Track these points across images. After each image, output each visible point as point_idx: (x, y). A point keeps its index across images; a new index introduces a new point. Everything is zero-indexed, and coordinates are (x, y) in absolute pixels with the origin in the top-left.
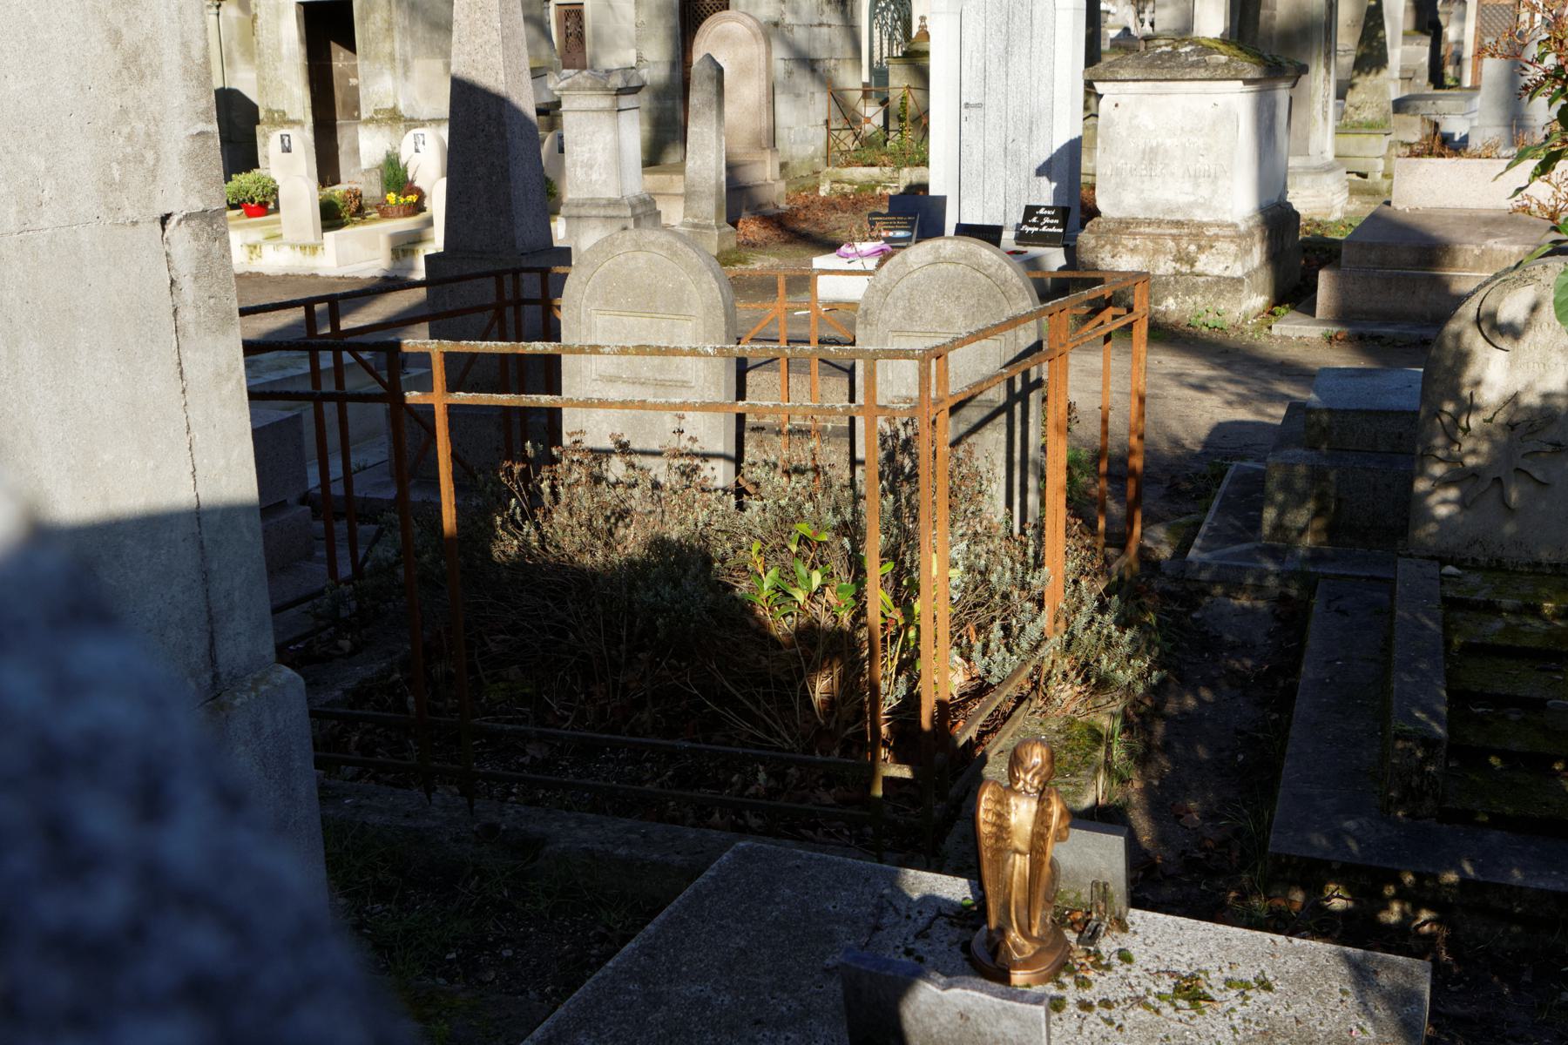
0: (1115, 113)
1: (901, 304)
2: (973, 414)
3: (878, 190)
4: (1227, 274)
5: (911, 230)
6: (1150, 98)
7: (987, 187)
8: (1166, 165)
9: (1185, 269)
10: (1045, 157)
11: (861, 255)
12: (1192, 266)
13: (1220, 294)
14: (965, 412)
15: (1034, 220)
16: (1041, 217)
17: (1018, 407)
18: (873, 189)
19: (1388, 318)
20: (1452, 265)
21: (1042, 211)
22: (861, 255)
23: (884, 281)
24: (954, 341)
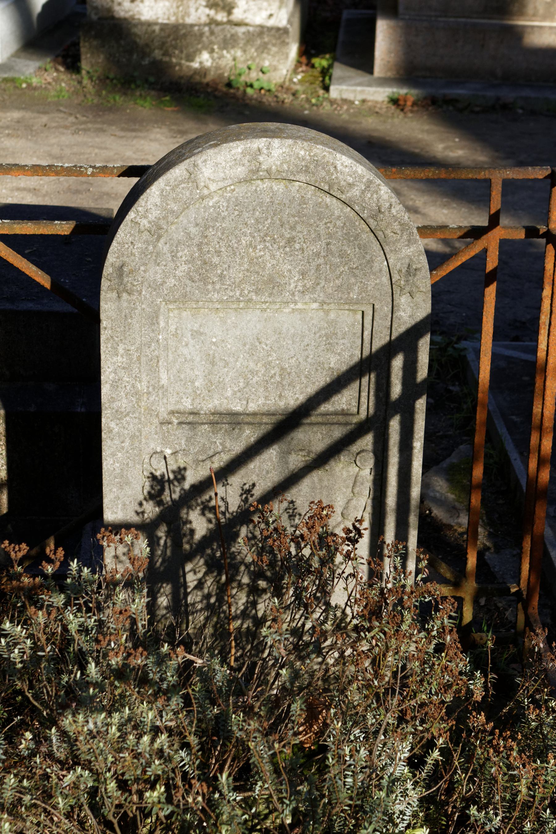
1: (184, 253)
2: (314, 437)
4: (271, 23)
9: (221, 17)
12: (230, 13)
13: (264, 48)
14: (300, 435)
17: (395, 424)
19: (455, 76)
20: (521, 13)
23: (154, 214)
24: (50, 166)
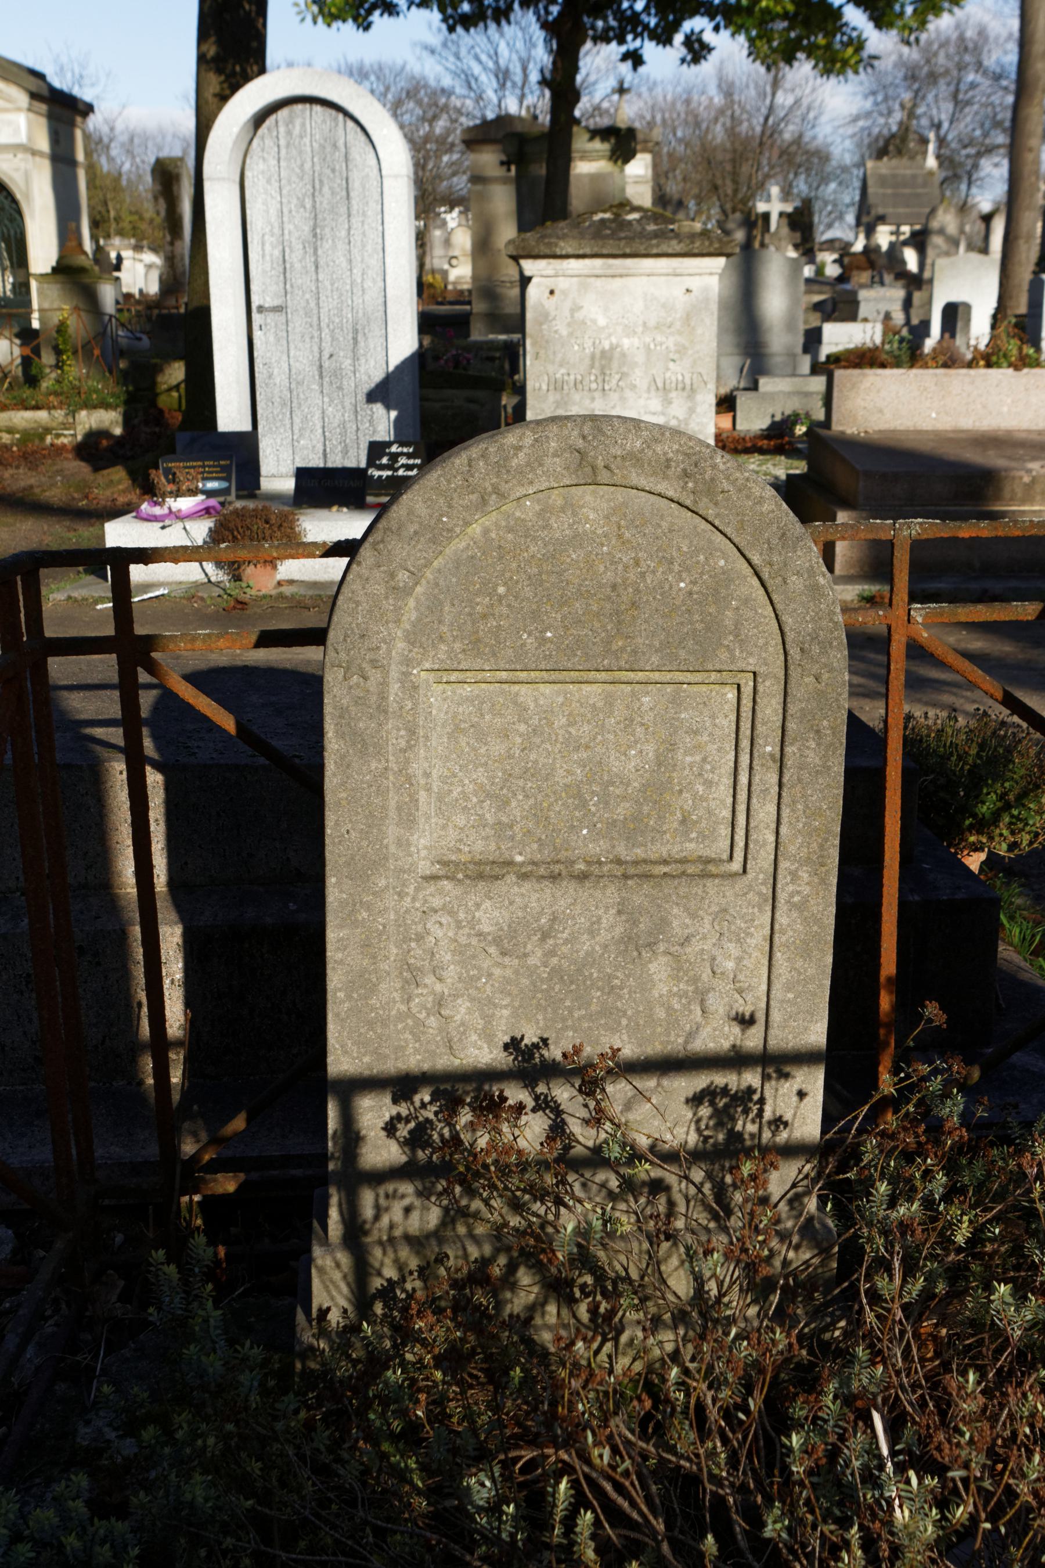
0: (550, 304)
3: (49, 439)
5: (227, 479)
6: (599, 283)
7: (297, 420)
8: (623, 376)
10: (378, 376)
11: (178, 516)
15: (385, 460)
16: (394, 457)
18: (42, 438)
20: (998, 497)
21: (394, 449)
22: (178, 516)
